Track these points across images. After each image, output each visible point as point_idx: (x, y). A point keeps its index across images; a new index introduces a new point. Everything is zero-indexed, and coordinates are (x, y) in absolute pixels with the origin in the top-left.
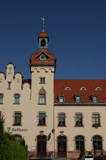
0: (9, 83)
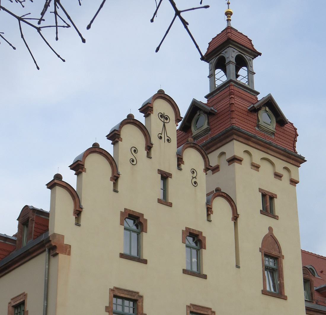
0: (165, 177)
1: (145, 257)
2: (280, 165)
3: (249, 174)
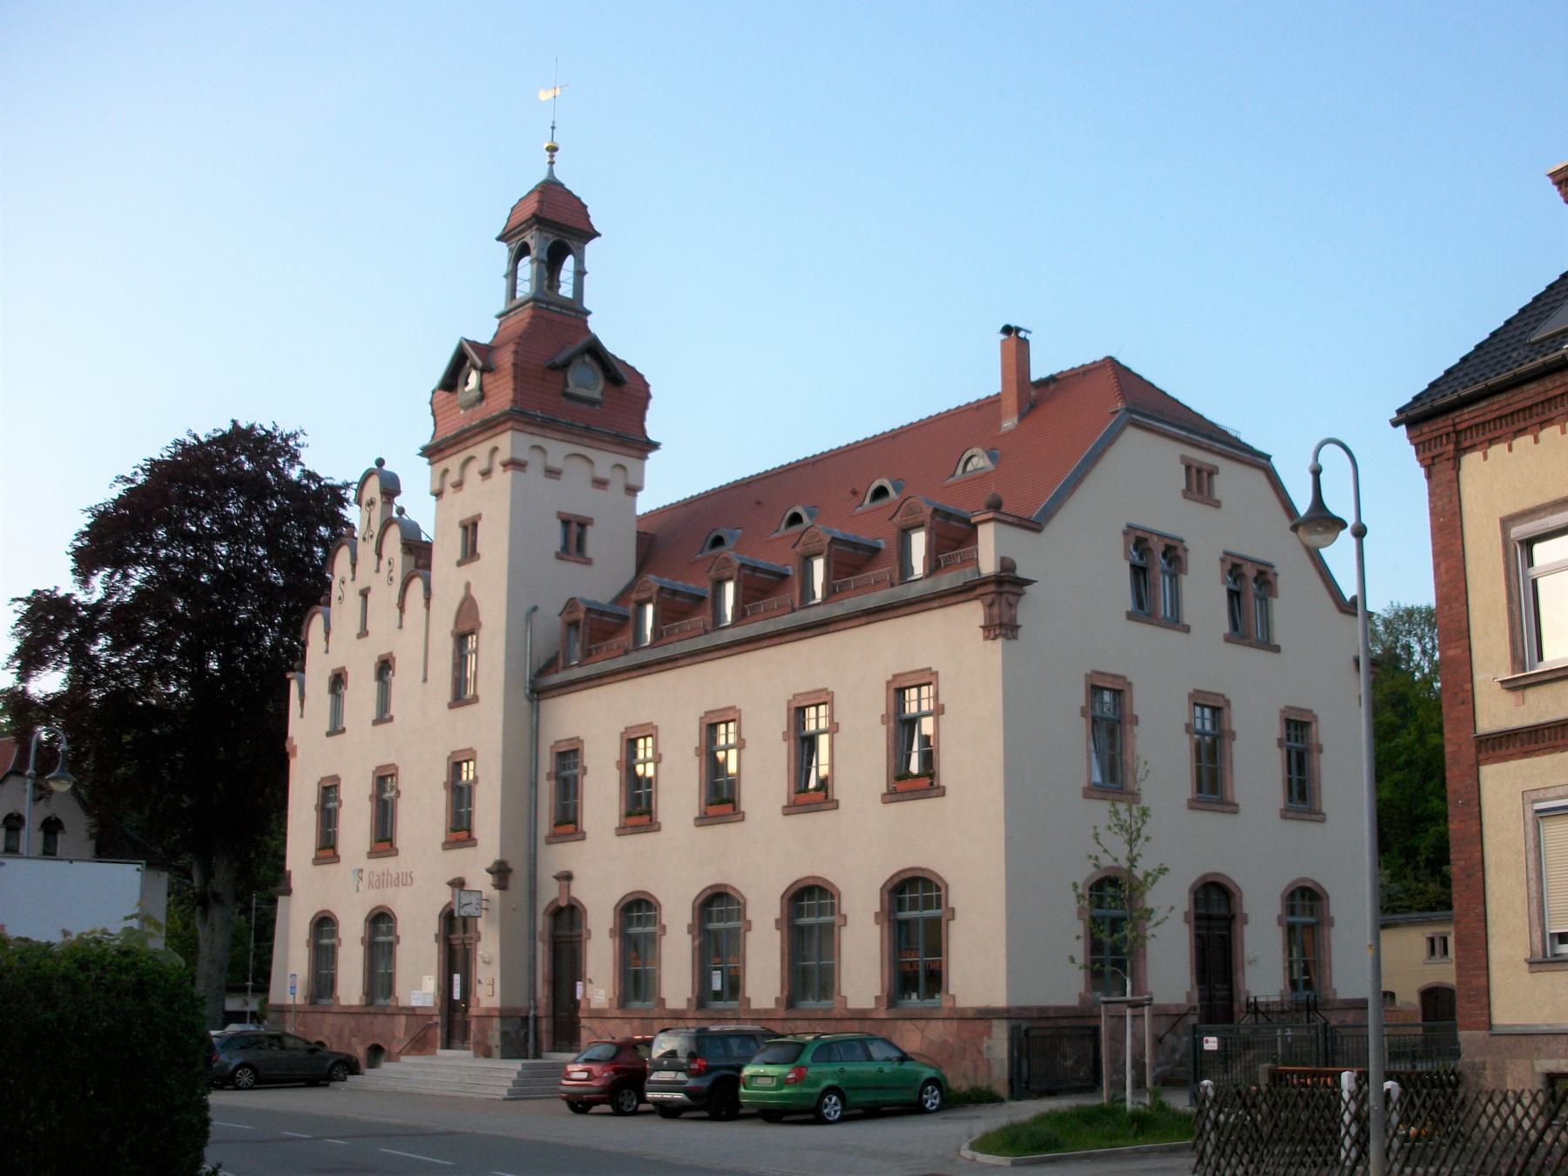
2: (605, 461)
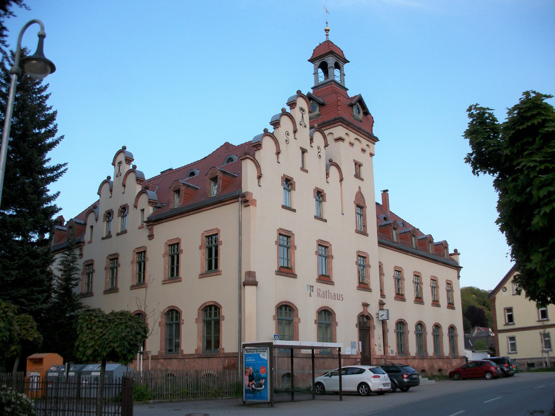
1: (325, 218)
3: (346, 147)
